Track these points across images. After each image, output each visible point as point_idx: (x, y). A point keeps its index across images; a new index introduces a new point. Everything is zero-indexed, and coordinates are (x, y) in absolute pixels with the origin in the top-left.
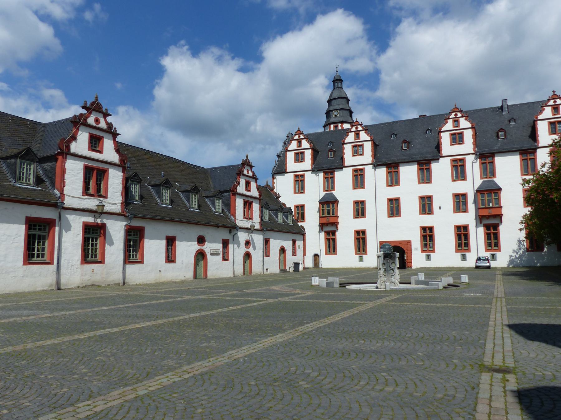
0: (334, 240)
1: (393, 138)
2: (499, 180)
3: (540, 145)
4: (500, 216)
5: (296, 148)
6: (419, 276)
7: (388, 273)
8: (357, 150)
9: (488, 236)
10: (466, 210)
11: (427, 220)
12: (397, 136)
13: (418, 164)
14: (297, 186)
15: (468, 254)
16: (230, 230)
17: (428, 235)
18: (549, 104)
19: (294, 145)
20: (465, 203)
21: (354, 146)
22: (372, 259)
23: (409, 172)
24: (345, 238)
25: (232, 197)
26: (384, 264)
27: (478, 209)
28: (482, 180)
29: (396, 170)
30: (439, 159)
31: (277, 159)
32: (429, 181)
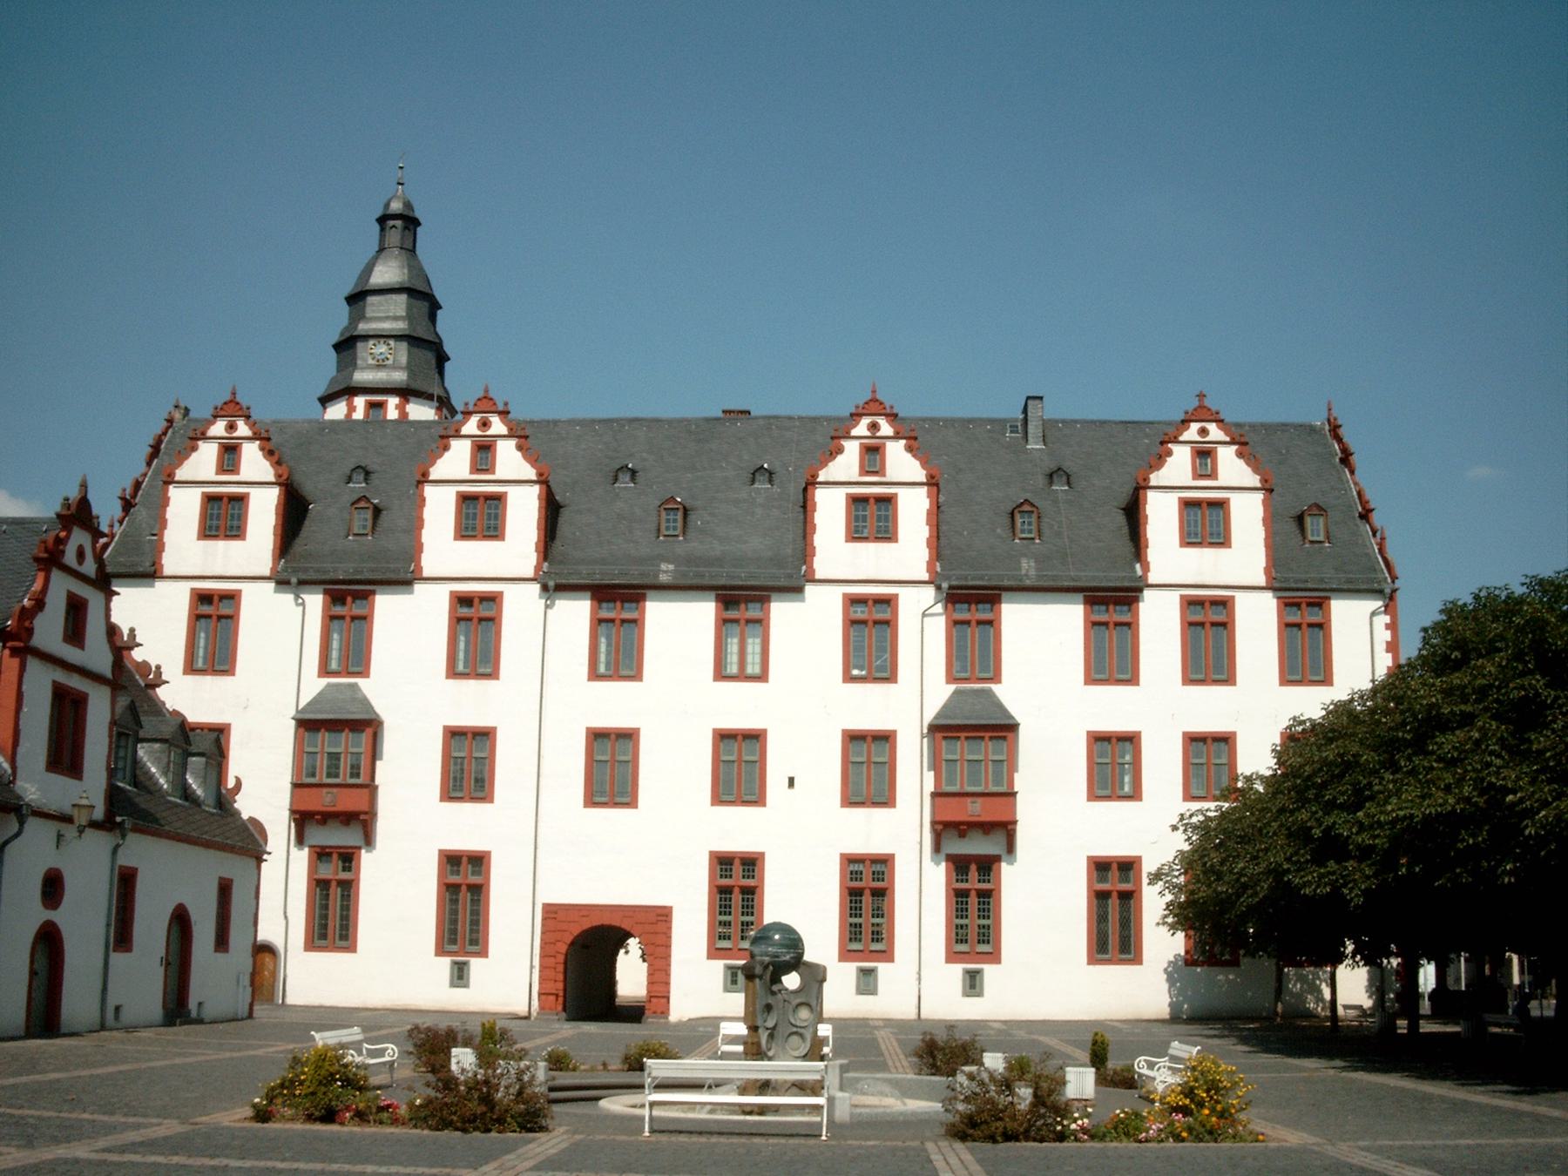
0: (349, 888)
2: (1012, 693)
4: (1006, 829)
8: (1205, 522)
11: (738, 829)
13: (719, 599)
18: (1185, 436)
23: (679, 628)
24: (396, 882)
28: (953, 687)
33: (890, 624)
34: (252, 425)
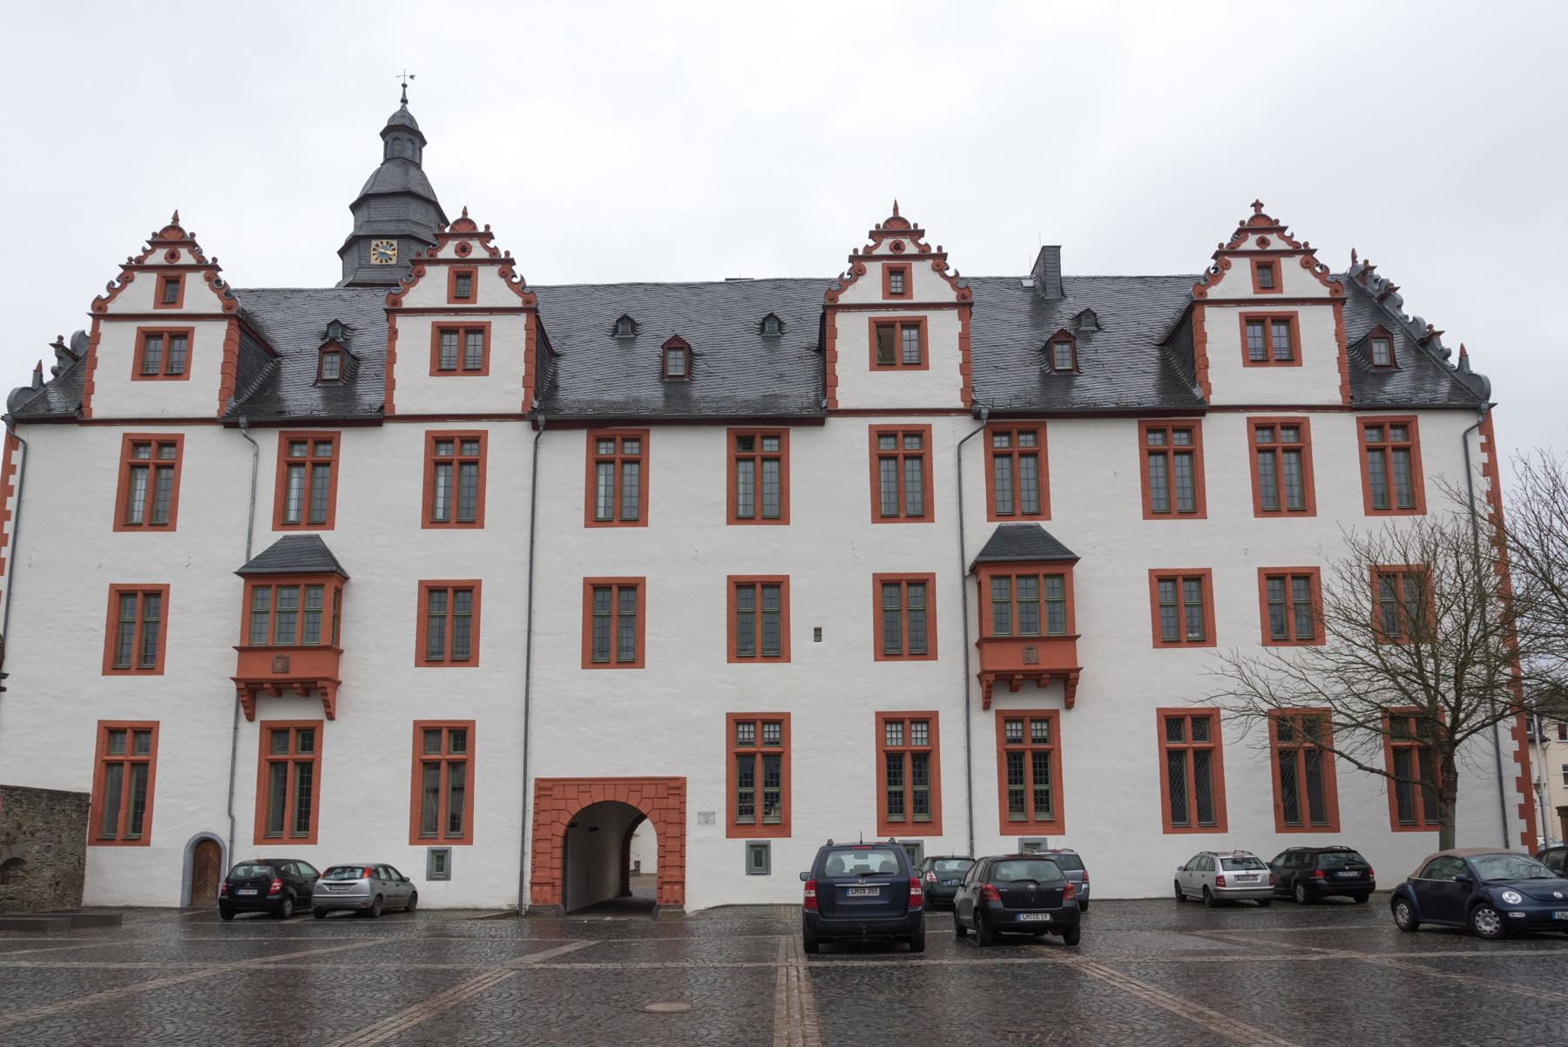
0: (308, 772)
3: (1215, 400)
4: (1066, 681)
5: (148, 307)
11: (761, 687)
15: (777, 844)
22: (492, 867)
23: (687, 468)
28: (280, 535)
33: (922, 458)
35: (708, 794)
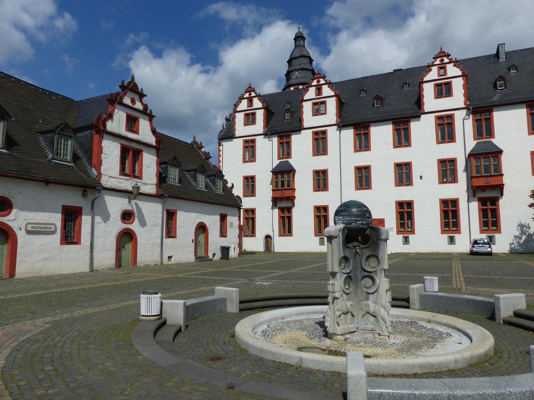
0: (290, 218)
1: (363, 94)
4: (500, 188)
5: (246, 108)
6: (427, 283)
7: (356, 285)
8: (319, 108)
9: (484, 213)
10: (455, 180)
11: (405, 194)
12: (368, 92)
13: (394, 123)
14: (247, 154)
15: (457, 236)
16: (85, 191)
17: (405, 212)
19: (243, 106)
20: (454, 172)
21: (314, 104)
23: (382, 134)
25: (96, 137)
26: (345, 259)
27: (470, 178)
28: (476, 142)
29: (366, 132)
30: (420, 117)
31: (225, 123)
32: (408, 143)
34: (256, 93)
35: (391, 223)
